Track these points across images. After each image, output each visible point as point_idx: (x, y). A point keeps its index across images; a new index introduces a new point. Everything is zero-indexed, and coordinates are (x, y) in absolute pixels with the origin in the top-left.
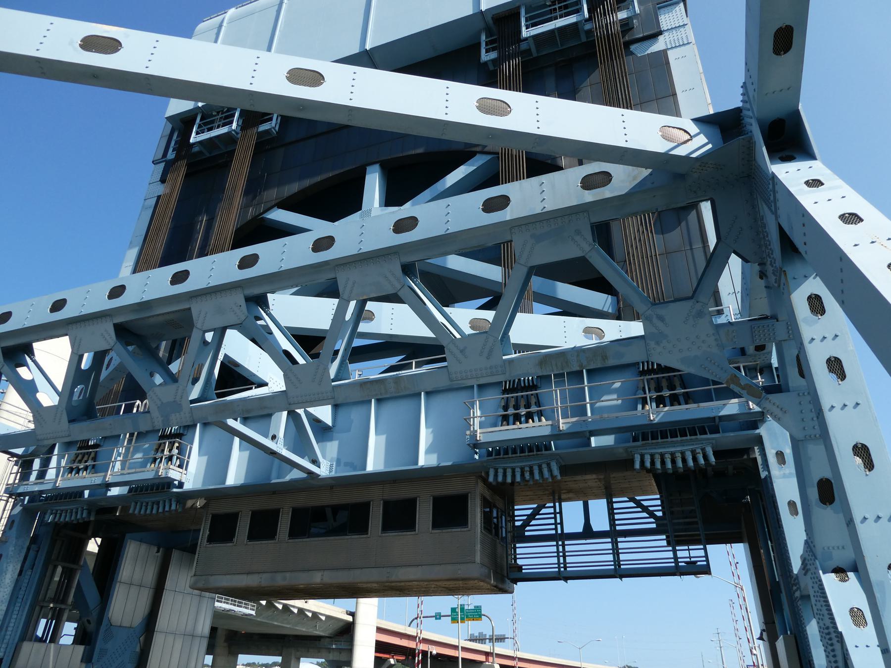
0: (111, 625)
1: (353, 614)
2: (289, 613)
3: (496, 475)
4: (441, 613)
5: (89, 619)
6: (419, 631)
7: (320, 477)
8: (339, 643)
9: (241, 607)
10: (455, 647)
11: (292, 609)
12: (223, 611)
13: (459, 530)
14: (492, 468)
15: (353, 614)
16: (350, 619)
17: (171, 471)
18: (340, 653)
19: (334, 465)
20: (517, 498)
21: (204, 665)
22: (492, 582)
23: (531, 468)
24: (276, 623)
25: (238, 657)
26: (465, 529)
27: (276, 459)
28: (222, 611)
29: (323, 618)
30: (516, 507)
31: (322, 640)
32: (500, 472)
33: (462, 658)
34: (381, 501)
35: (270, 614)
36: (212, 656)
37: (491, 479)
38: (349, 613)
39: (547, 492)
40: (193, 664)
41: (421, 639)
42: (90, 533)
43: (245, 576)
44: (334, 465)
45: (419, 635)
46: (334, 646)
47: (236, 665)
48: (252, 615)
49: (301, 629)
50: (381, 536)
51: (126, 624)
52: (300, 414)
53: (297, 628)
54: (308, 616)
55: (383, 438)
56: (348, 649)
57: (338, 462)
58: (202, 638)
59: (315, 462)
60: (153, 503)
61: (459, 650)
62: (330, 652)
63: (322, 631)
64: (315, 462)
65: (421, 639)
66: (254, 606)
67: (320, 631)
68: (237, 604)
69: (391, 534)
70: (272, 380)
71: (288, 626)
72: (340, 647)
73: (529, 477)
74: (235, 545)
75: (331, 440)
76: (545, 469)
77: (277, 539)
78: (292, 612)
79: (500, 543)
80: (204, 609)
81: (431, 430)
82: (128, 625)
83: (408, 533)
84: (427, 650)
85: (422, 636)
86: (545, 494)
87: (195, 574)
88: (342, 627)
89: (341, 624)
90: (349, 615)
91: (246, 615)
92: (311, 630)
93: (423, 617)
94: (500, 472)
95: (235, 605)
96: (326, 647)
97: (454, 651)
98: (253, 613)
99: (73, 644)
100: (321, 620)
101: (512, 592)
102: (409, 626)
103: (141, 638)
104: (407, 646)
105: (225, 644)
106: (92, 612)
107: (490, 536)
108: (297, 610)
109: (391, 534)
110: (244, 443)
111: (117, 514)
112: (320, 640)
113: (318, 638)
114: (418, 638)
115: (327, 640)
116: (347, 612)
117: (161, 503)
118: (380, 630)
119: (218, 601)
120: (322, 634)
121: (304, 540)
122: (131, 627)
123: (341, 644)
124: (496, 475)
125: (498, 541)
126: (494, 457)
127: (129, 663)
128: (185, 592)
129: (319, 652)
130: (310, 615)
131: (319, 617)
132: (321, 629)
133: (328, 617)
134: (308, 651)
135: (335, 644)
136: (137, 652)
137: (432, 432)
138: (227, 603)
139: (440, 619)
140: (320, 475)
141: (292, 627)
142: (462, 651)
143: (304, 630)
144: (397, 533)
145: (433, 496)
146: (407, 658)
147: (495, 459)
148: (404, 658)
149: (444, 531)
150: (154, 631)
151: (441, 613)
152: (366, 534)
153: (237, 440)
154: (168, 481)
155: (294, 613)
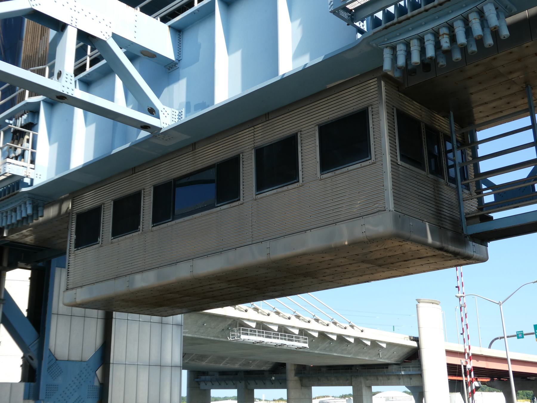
0: (57, 360)
1: (416, 340)
2: (329, 341)
3: (394, 58)
4: (522, 331)
5: (31, 355)
6: (467, 347)
7: (162, 131)
8: (407, 369)
9: (292, 341)
10: (504, 360)
11: (348, 339)
12: (275, 346)
13: (358, 165)
14: (387, 47)
15: (416, 340)
16: (414, 344)
17: (8, 166)
18: (411, 379)
19: (183, 113)
20: (478, 113)
21: (181, 398)
22: (430, 240)
23: (451, 28)
24: (335, 354)
25: (311, 389)
26: (367, 163)
27: (119, 123)
28: (252, 344)
29: (384, 346)
30: (481, 135)
31: (390, 367)
32: (401, 49)
33: (513, 372)
34: (252, 150)
35: (327, 345)
36: (286, 390)
37: (387, 66)
38: (412, 338)
39: (516, 89)
40: (166, 396)
41: (470, 355)
42: (5, 264)
43: (112, 282)
44: (183, 113)
45: (468, 351)
46: (403, 373)
47: (310, 399)
48: (306, 348)
49: (314, 351)
50: (256, 200)
51: (75, 356)
52: (105, 41)
53: (359, 357)
54: (367, 345)
55: (238, 55)
56: (418, 374)
57: (188, 106)
58: (173, 368)
59: (152, 111)
60: (12, 211)
61: (508, 363)
62: (400, 379)
63: (388, 359)
64: (152, 111)
65: (470, 355)
66: (306, 339)
67: (384, 359)
68: (280, 337)
69: (268, 193)
70: (109, 25)
71: (349, 356)
72: (410, 373)
73: (448, 45)
74: (101, 246)
75: (177, 80)
76: (474, 21)
77: (141, 231)
78: (349, 342)
79: (447, 185)
80: (170, 335)
81: (298, 22)
82: (78, 359)
83: (290, 187)
84: (460, 364)
85: (472, 352)
86: (514, 94)
87: (68, 287)
88: (408, 353)
89: (406, 350)
90: (413, 340)
91: (300, 348)
92: (374, 358)
93: (508, 337)
94: (401, 49)
95: (285, 339)
96: (395, 374)
97: (485, 362)
98: (306, 345)
99: (20, 382)
100: (382, 347)
101: (484, 259)
102: (490, 347)
103: (97, 372)
104: (486, 367)
105: (296, 378)
106: (30, 347)
107: (423, 173)
108: (298, 331)
109: (268, 193)
110: (90, 114)
111: (5, 235)
112: (387, 368)
113: (385, 366)
114: (466, 354)
115: (395, 367)
116: (410, 338)
117: (18, 208)
118: (449, 353)
119: (243, 334)
120: (387, 361)
121: (169, 224)
122: (81, 361)
123: (410, 370)
124: (394, 58)
125: (442, 180)
126: (383, 26)
127: (46, 398)
128: (140, 320)
129: (389, 379)
130: (369, 343)
131: (379, 345)
132: (385, 357)
133: (389, 344)
134: (378, 379)
135: (404, 371)
136: (96, 386)
137: (300, 24)
138: (299, 341)
139: (523, 337)
140: (161, 129)
141: (354, 357)
142: (512, 364)
143: (367, 358)
144: (275, 191)
145: (318, 125)
146: (492, 380)
147: (386, 28)
148: (489, 380)
149: (338, 172)
150: (110, 363)
151: (522, 331)
152: (238, 200)
153: (79, 113)
154: (15, 180)
155: (351, 343)
